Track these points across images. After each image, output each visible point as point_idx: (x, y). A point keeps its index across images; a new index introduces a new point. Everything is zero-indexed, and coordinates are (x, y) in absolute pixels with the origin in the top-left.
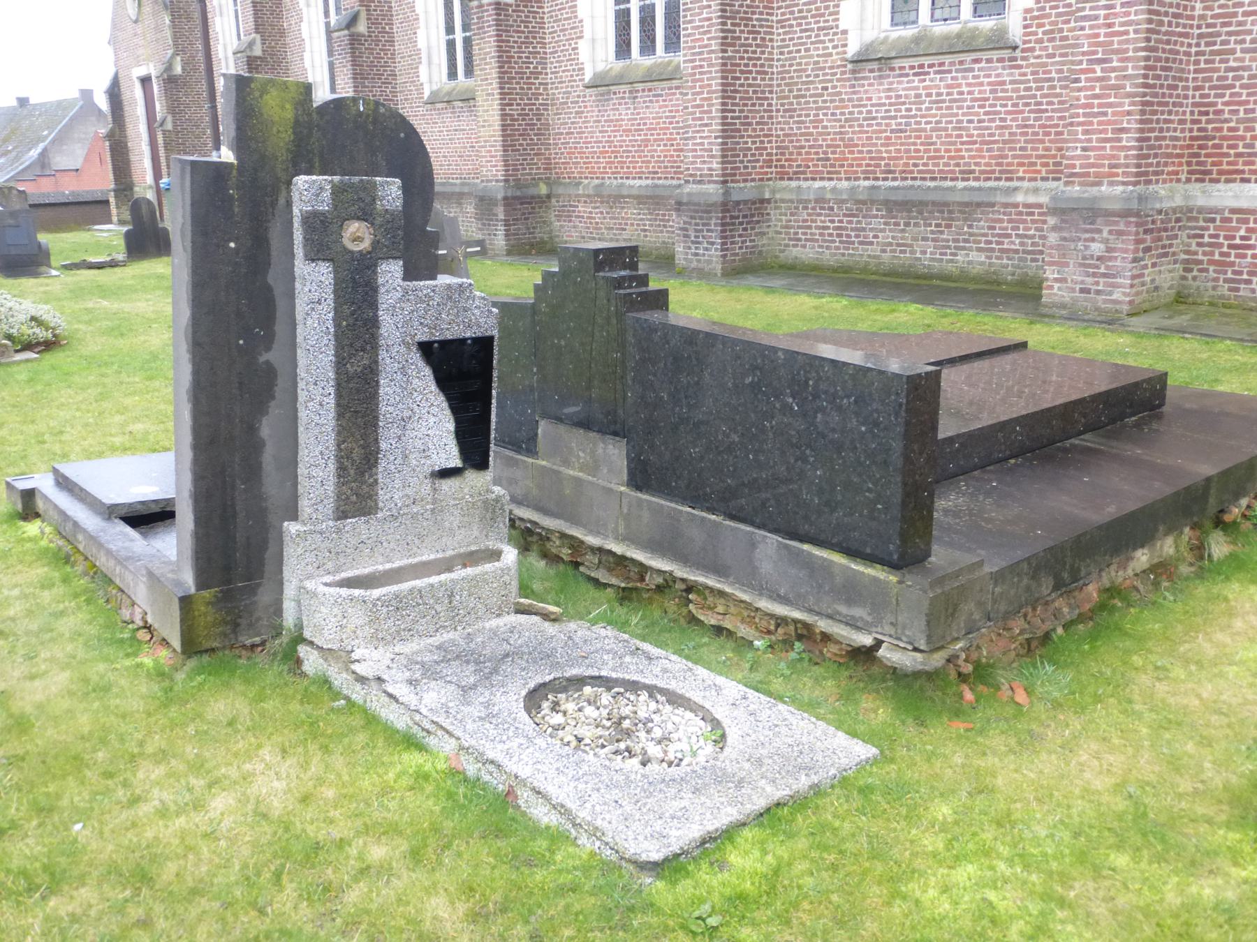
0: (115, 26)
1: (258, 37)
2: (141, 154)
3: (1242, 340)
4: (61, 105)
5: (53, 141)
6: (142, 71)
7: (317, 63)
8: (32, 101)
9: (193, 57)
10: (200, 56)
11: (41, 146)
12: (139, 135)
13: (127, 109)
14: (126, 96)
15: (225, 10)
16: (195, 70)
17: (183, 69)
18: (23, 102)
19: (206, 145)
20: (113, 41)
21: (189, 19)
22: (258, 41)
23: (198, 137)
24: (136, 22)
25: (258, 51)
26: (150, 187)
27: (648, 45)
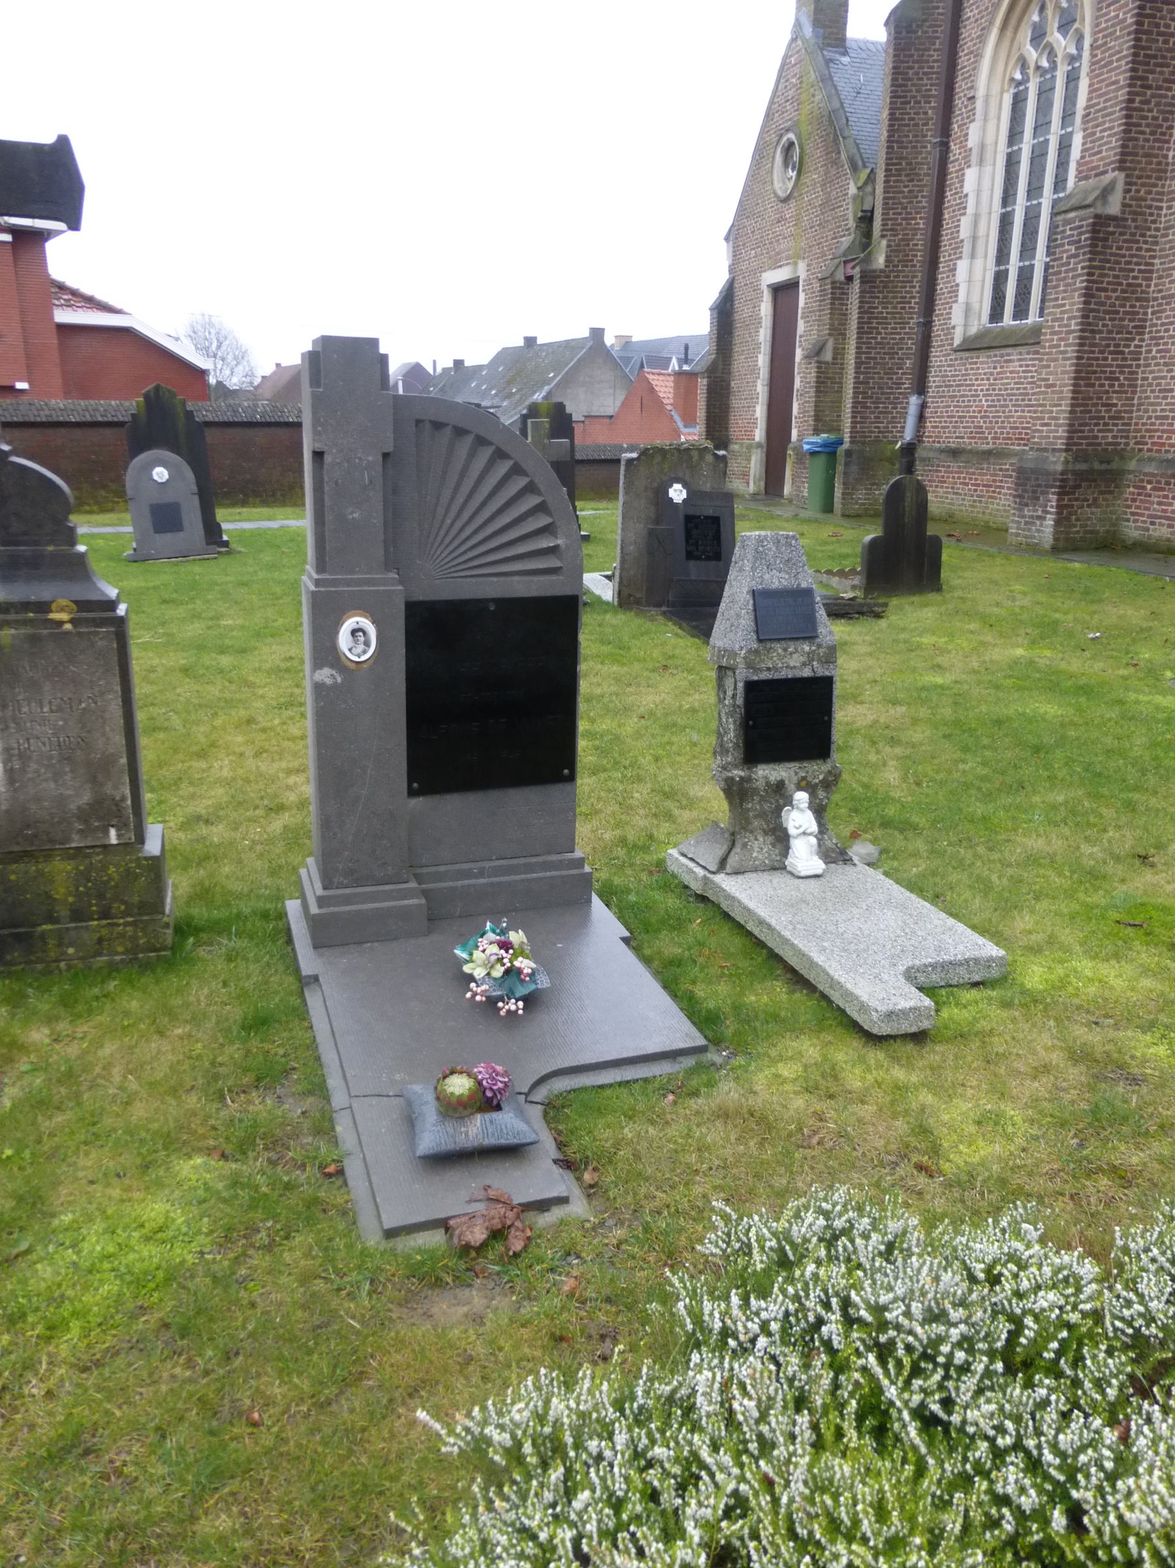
0: (745, 210)
1: (1121, 177)
2: (753, 398)
3: (858, 516)
4: (569, 346)
5: (558, 385)
6: (780, 275)
7: (978, 275)
8: (539, 342)
9: (906, 240)
10: (920, 241)
11: (547, 388)
12: (754, 369)
13: (739, 334)
14: (742, 312)
15: (989, 155)
16: (906, 262)
17: (888, 260)
18: (530, 341)
19: (899, 384)
20: (735, 236)
21: (913, 176)
22: (1120, 187)
23: (890, 372)
24: (786, 200)
25: (1114, 207)
26: (759, 445)
27: (1021, 311)
